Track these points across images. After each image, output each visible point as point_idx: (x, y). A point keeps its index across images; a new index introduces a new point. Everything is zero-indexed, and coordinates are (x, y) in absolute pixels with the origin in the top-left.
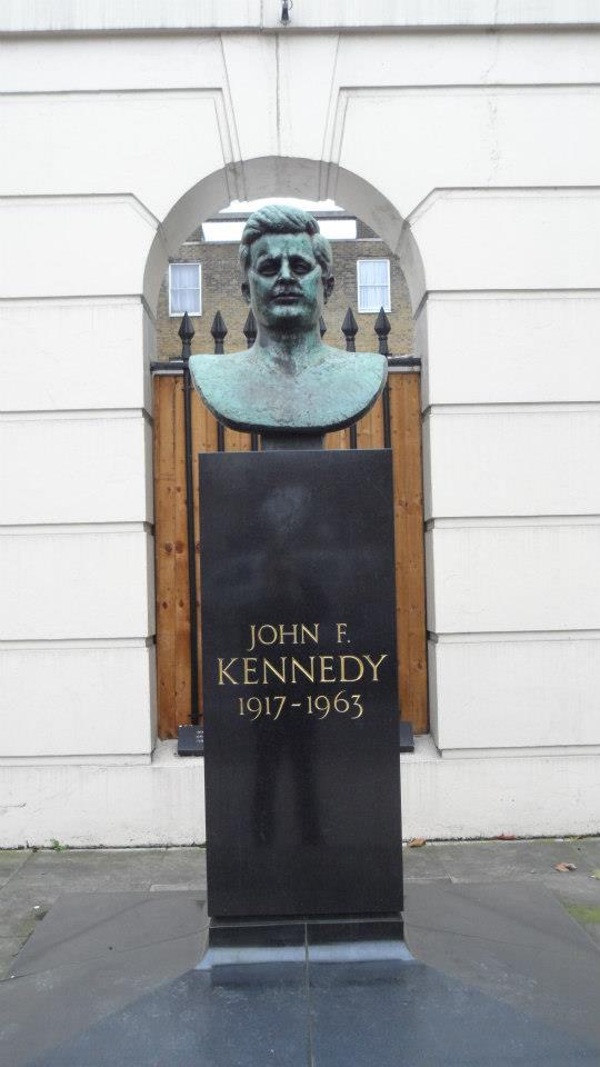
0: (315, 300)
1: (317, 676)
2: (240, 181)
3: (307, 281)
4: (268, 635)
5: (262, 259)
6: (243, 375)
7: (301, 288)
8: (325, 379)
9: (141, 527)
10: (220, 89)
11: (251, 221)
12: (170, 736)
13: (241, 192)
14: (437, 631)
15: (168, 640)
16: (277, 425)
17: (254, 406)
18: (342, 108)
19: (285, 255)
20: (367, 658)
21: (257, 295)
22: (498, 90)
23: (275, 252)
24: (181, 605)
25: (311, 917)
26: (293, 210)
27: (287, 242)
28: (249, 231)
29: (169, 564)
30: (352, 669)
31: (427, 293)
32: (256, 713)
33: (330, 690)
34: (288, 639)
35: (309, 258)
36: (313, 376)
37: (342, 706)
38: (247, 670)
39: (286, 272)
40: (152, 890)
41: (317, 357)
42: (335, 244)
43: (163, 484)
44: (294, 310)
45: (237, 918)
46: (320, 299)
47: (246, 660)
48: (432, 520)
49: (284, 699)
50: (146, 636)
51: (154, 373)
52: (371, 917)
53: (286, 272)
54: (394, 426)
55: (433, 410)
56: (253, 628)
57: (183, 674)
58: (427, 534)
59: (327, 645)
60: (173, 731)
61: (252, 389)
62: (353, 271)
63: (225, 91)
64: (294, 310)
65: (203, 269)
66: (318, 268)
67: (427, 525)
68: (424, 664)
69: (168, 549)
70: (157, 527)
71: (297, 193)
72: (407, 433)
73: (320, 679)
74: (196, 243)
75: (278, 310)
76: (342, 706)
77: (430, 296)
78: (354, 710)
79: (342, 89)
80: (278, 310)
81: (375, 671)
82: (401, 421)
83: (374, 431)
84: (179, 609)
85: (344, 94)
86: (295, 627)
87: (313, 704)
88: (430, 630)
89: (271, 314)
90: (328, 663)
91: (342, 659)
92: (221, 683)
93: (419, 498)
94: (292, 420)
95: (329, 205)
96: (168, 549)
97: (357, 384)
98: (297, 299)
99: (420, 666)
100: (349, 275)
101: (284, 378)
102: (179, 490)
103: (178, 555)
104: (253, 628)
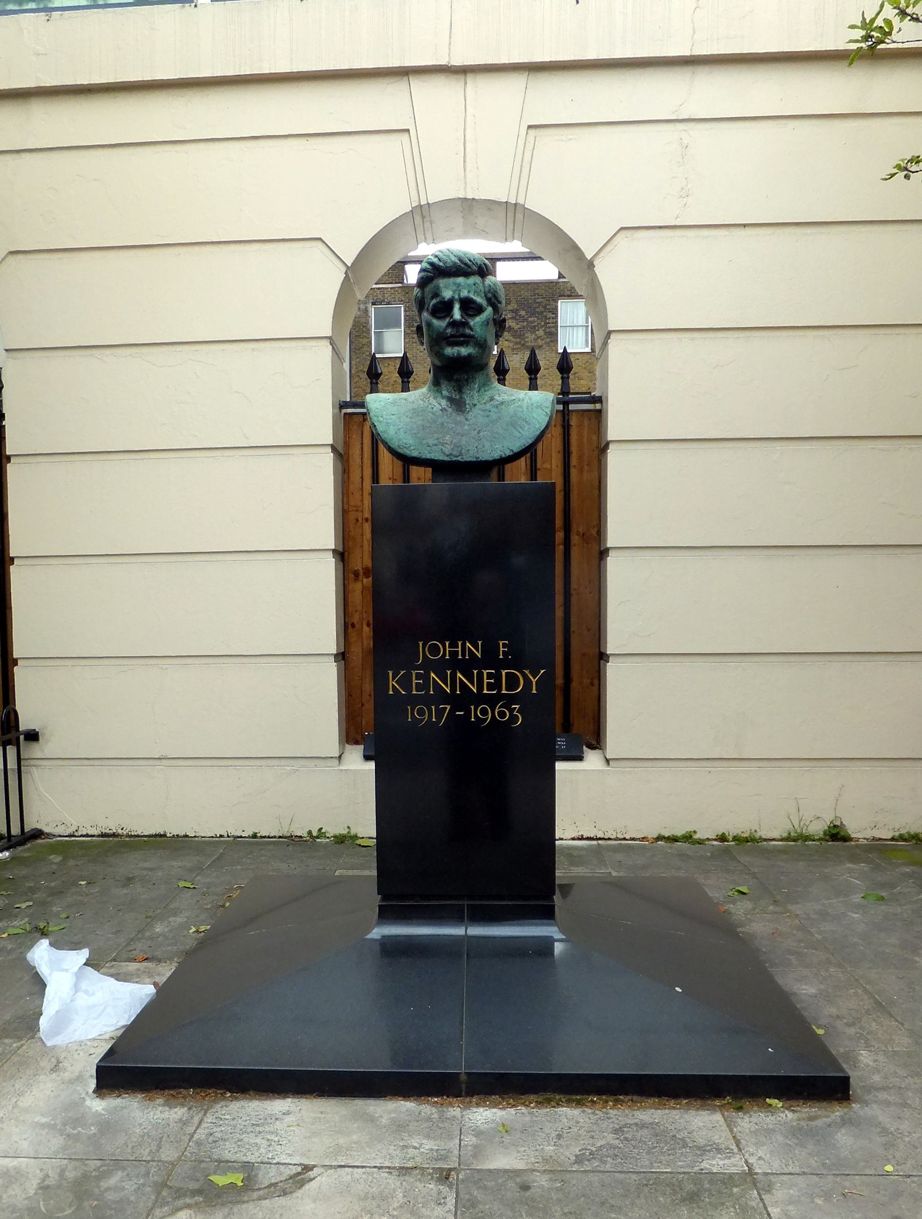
0: (485, 341)
1: (480, 687)
2: (427, 225)
3: (476, 322)
4: (435, 650)
5: (434, 301)
6: (416, 412)
7: (471, 329)
8: (494, 416)
9: (331, 554)
10: (408, 131)
11: (425, 265)
12: (357, 743)
13: (429, 235)
14: (608, 653)
15: (357, 653)
16: (446, 459)
17: (425, 442)
18: (530, 146)
19: (457, 297)
20: (527, 672)
21: (429, 335)
22: (691, 125)
23: (447, 294)
24: (368, 625)
25: (471, 898)
26: (465, 254)
27: (459, 285)
28: (423, 274)
29: (357, 588)
30: (512, 682)
31: (610, 333)
32: (487, 718)
33: (492, 701)
34: (454, 654)
35: (479, 300)
36: (482, 413)
37: (502, 714)
38: (414, 681)
39: (457, 314)
40: (337, 874)
41: (489, 394)
42: (507, 285)
43: (352, 516)
44: (464, 351)
45: (403, 897)
46: (491, 338)
47: (414, 673)
48: (607, 550)
49: (449, 707)
50: (335, 653)
51: (344, 411)
52: (525, 900)
53: (457, 314)
54: (574, 461)
55: (611, 446)
56: (421, 644)
57: (368, 687)
58: (602, 562)
59: (490, 659)
60: (359, 738)
61: (423, 426)
62: (555, 311)
63: (412, 132)
64: (464, 351)
65: (405, 311)
66: (489, 310)
67: (603, 553)
68: (596, 682)
69: (356, 574)
70: (346, 554)
71: (484, 234)
72: (586, 468)
73: (483, 690)
74: (400, 285)
75: (449, 351)
76: (502, 714)
77: (613, 336)
78: (513, 718)
79: (530, 127)
80: (449, 351)
81: (534, 683)
82: (580, 457)
83: (554, 466)
84: (366, 629)
85: (532, 132)
86: (460, 643)
87: (475, 713)
88: (602, 650)
89: (443, 355)
90: (490, 676)
91: (504, 673)
92: (391, 693)
93: (596, 529)
94: (461, 454)
95: (516, 247)
96: (356, 574)
97: (525, 420)
98: (466, 340)
99: (592, 684)
100: (550, 315)
101: (454, 415)
102: (367, 520)
103: (365, 580)
104: (421, 644)
